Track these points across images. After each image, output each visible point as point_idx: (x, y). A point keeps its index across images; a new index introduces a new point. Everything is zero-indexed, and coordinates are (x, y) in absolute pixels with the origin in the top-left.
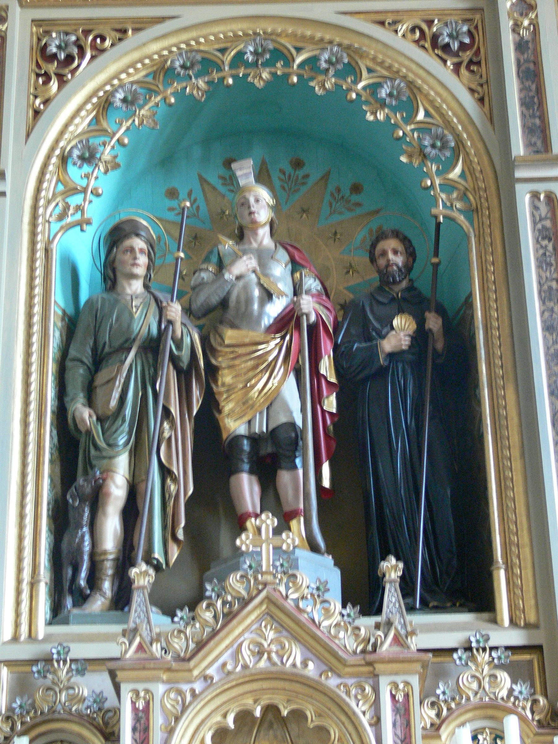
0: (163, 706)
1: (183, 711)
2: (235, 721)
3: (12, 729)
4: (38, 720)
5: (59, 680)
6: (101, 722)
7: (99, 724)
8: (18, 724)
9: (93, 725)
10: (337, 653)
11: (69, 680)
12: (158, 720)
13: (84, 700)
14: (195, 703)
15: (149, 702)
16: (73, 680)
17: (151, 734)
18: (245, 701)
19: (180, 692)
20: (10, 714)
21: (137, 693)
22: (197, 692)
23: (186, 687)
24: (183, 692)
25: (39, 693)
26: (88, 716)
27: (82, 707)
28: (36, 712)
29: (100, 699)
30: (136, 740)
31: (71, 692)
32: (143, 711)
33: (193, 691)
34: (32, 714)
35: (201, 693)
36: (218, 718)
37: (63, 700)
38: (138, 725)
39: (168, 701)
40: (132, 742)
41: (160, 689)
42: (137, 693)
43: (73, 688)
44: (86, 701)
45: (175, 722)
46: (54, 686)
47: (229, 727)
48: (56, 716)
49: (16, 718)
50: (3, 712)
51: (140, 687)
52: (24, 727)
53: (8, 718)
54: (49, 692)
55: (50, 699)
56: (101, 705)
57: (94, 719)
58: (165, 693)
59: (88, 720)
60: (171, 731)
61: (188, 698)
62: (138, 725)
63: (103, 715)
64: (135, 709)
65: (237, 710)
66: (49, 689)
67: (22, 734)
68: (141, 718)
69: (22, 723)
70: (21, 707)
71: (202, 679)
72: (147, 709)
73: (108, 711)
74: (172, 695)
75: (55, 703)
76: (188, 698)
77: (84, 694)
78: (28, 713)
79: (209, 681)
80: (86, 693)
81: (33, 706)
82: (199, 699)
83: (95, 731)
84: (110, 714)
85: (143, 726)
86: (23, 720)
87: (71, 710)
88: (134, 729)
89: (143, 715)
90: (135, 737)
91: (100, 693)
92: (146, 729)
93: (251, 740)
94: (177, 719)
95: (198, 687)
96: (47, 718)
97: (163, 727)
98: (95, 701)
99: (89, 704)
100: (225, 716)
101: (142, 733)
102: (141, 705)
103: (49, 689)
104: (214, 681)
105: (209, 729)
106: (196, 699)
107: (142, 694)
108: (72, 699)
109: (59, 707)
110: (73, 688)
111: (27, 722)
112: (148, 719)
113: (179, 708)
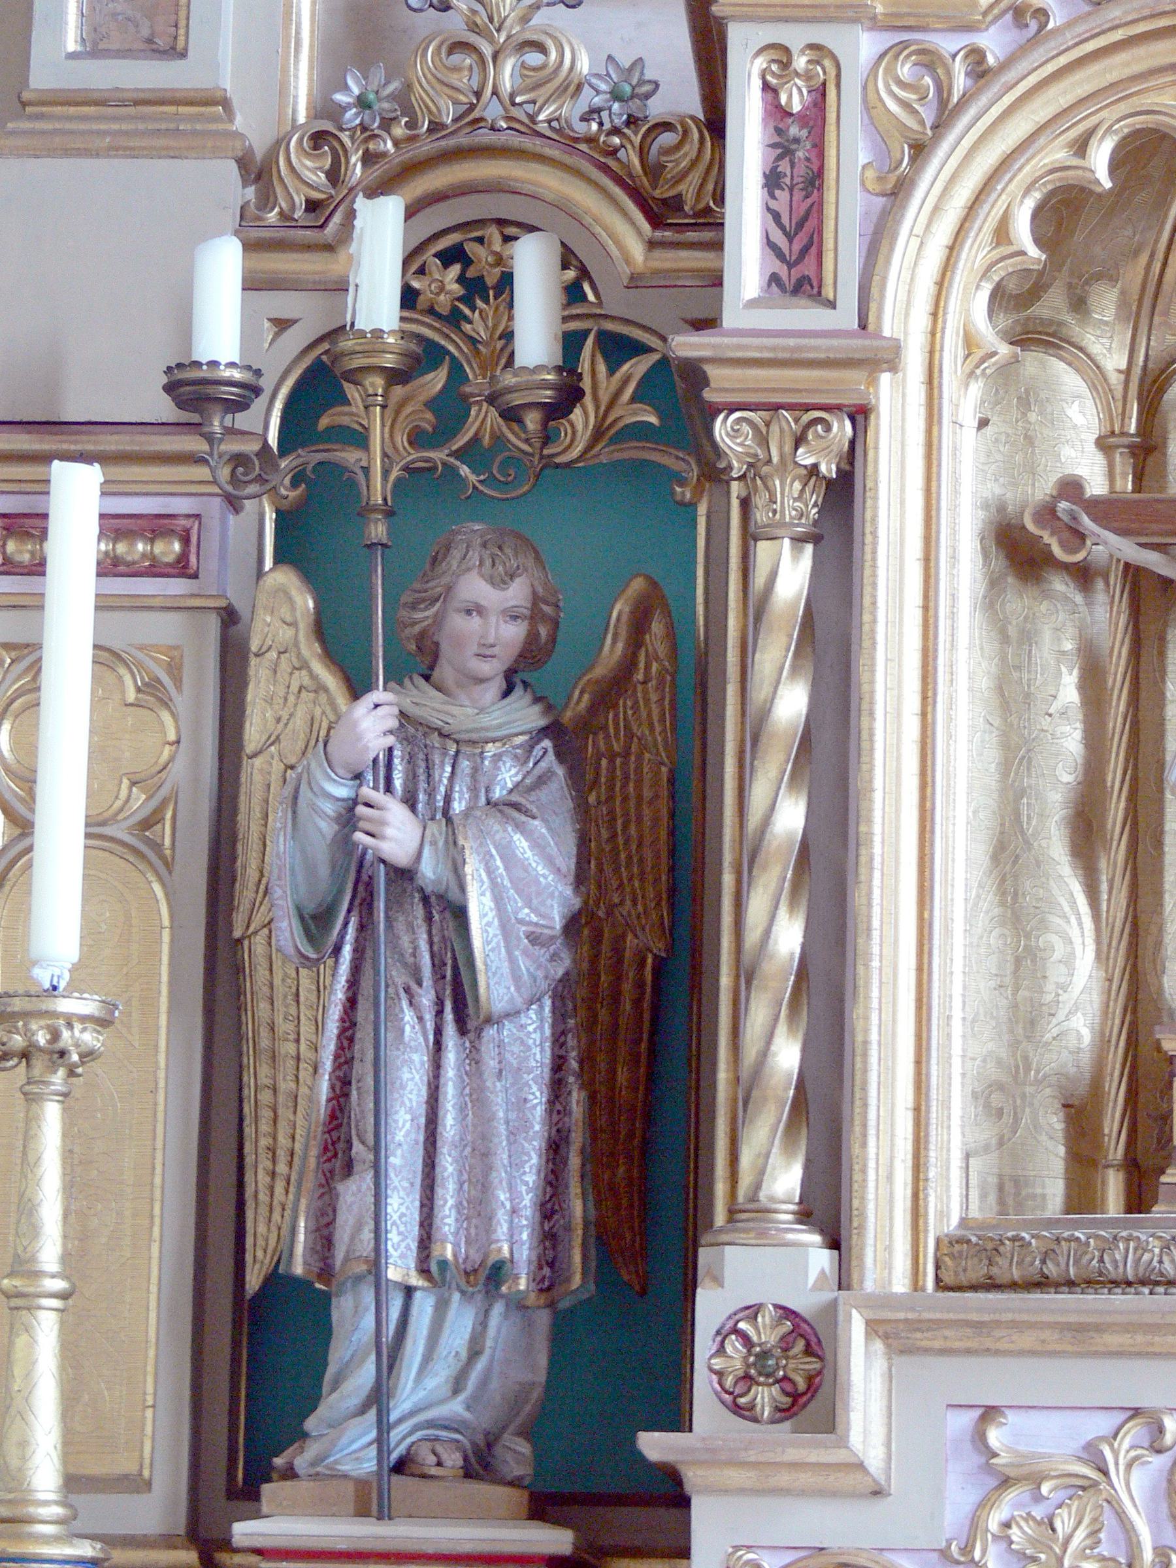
0: (871, 106)
1: (940, 126)
2: (1114, 167)
3: (334, 175)
4: (426, 147)
5: (491, 20)
6: (636, 161)
7: (627, 167)
8: (353, 160)
9: (605, 169)
10: (998, 182)
11: (525, 19)
12: (853, 153)
13: (579, 87)
14: (984, 100)
15: (822, 91)
16: (538, 19)
17: (830, 196)
18: (1150, 100)
19: (930, 60)
20: (328, 126)
21: (781, 55)
22: (991, 60)
23: (948, 43)
24: (940, 57)
25: (424, 55)
26: (591, 140)
27: (571, 110)
28: (412, 125)
29: (632, 86)
30: (776, 217)
31: (534, 58)
32: (802, 119)
33: (976, 56)
34: (399, 131)
35: (1004, 66)
36: (1057, 153)
37: (507, 85)
38: (784, 166)
39: (887, 86)
40: (763, 217)
41: (861, 47)
42: (781, 55)
43: (541, 48)
44: (587, 91)
45: (913, 159)
46: (473, 39)
47: (1098, 182)
48: (484, 137)
49: (345, 137)
50: (302, 119)
51: (795, 37)
52: (377, 171)
53: (319, 139)
54: (456, 58)
55: (461, 80)
56: (634, 106)
57: (613, 152)
58: (882, 56)
59: (593, 154)
60: (897, 192)
61: (960, 82)
62: (784, 166)
63: (644, 137)
64: (777, 112)
65: (1124, 127)
66: (460, 46)
67: (374, 191)
68: (797, 141)
69: (369, 159)
70: (362, 103)
71: (1009, 16)
72: (817, 114)
73: (666, 126)
74: (905, 70)
75: (478, 94)
76: (960, 82)
77: (578, 65)
78: (387, 123)
79: (1033, 25)
80: (584, 66)
81: (403, 99)
82: (996, 88)
83: (617, 191)
84: (667, 139)
85: (801, 170)
86: (371, 146)
87: (532, 118)
88: (772, 181)
89: (804, 133)
90: (773, 205)
91: (634, 64)
92: (815, 180)
93: (1160, 232)
94: (920, 150)
95: (994, 42)
96: (452, 142)
97: (870, 174)
98: (616, 96)
99: (598, 101)
100: (1081, 147)
101: (798, 195)
102: (795, 99)
103: (460, 46)
104: (1051, 25)
105: (1027, 191)
106: (987, 85)
107: (800, 62)
108: (534, 80)
109: (492, 111)
110: (541, 48)
111: (384, 154)
112: (819, 148)
113: (928, 114)
